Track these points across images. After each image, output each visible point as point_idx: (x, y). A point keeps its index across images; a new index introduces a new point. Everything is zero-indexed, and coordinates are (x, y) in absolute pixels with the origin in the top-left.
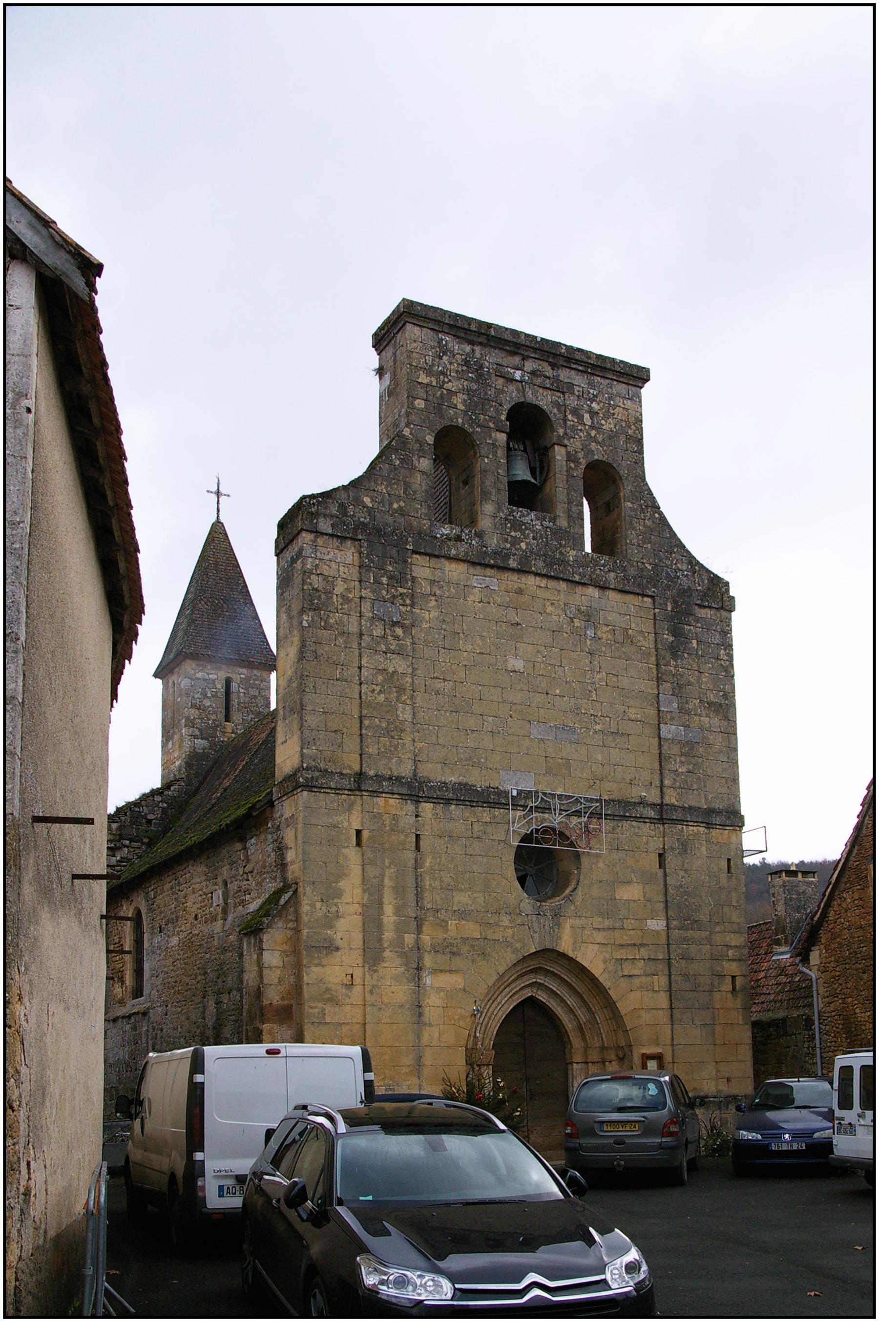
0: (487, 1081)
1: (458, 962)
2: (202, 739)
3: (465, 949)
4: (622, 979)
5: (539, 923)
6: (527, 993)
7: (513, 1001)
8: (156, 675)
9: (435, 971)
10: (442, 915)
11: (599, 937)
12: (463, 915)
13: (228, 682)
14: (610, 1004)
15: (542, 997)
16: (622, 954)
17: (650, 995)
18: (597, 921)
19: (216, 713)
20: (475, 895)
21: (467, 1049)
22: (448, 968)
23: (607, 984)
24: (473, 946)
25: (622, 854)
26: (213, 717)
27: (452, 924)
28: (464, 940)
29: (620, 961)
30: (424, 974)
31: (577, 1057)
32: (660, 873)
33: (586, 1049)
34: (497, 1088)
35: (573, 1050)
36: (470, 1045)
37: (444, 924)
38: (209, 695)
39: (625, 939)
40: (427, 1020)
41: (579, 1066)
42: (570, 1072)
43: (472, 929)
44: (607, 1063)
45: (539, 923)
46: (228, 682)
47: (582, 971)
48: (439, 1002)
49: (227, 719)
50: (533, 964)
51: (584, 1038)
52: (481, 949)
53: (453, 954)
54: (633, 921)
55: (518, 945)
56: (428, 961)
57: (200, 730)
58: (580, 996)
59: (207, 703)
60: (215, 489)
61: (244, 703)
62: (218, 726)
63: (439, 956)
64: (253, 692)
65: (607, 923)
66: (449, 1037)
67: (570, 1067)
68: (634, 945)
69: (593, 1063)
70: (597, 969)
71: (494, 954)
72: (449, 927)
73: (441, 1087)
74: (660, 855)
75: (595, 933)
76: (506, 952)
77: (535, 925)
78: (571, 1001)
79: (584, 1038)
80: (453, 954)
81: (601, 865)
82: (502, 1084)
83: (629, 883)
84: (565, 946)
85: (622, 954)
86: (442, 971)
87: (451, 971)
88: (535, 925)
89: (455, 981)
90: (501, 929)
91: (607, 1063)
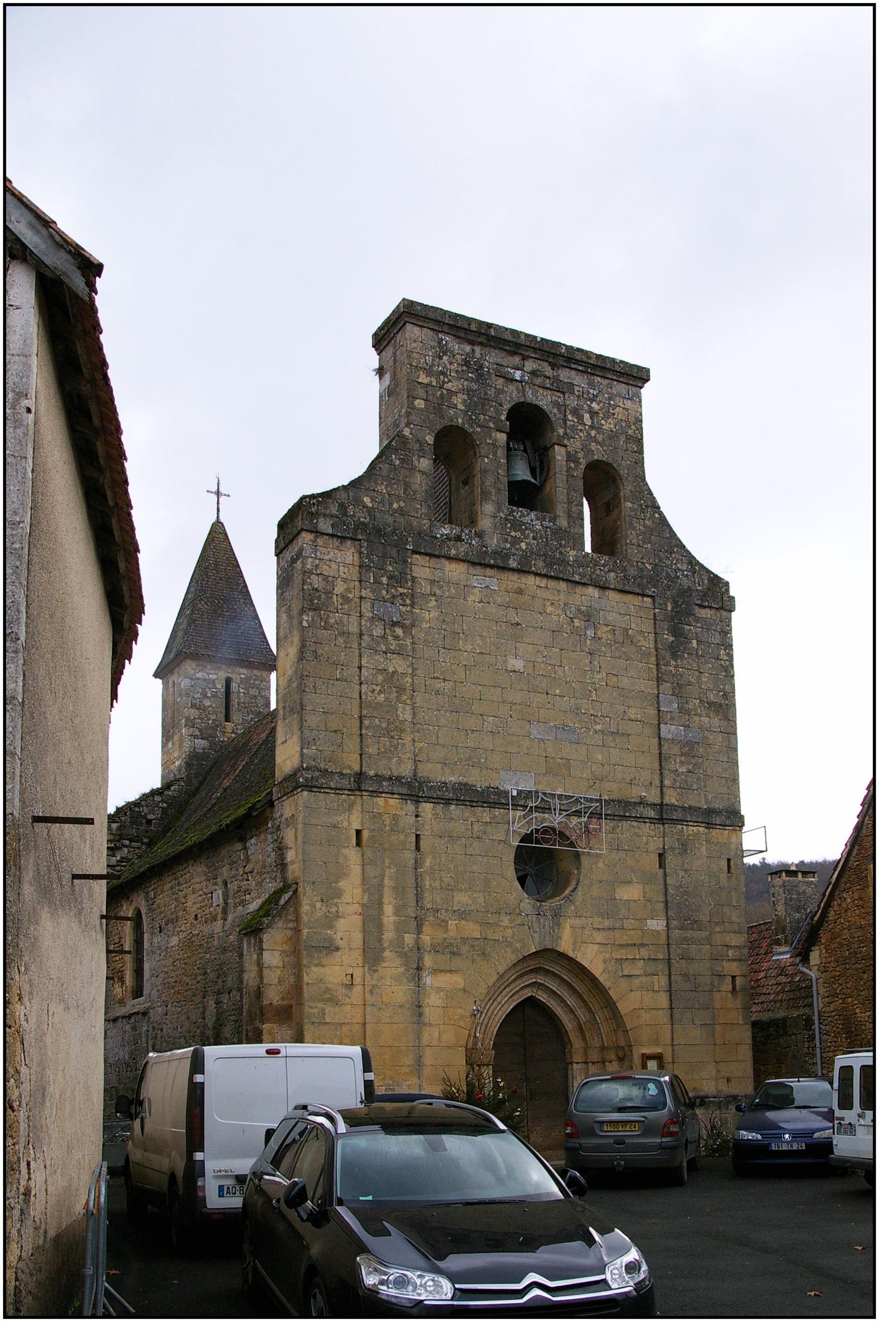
0: (487, 1081)
1: (458, 962)
2: (202, 739)
3: (465, 949)
4: (622, 979)
5: (539, 923)
6: (527, 993)
7: (513, 1001)
8: (156, 675)
9: (435, 971)
10: (442, 915)
11: (599, 937)
12: (463, 915)
13: (228, 682)
14: (610, 1005)
15: (542, 997)
16: (622, 954)
17: (650, 996)
18: (597, 921)
19: (216, 713)
20: (475, 895)
21: (467, 1049)
22: (448, 968)
23: (607, 984)
24: (473, 946)
25: (622, 854)
26: (213, 717)
27: (452, 924)
28: (464, 940)
29: (620, 961)
30: (424, 974)
31: (577, 1057)
32: (660, 872)
33: (586, 1049)
34: (497, 1088)
35: (573, 1051)
36: (470, 1045)
37: (444, 924)
38: (209, 695)
39: (626, 940)
40: (426, 1020)
41: (579, 1066)
42: (570, 1072)
43: (472, 929)
44: (607, 1063)
45: (539, 923)
46: (228, 682)
47: (582, 971)
48: (439, 1002)
49: (227, 719)
50: (533, 964)
51: (584, 1038)
52: (481, 949)
53: (453, 953)
54: (633, 921)
55: (518, 945)
56: (428, 961)
57: (200, 730)
58: (580, 997)
59: (207, 703)
60: (215, 489)
61: (244, 703)
62: (218, 726)
63: (439, 956)
64: (253, 692)
65: (607, 923)
66: (449, 1037)
67: (570, 1067)
68: (634, 945)
69: (593, 1063)
70: (597, 969)
71: (494, 955)
72: (449, 928)
73: (441, 1087)
74: (660, 855)
75: (595, 933)
76: (506, 952)
77: (535, 925)
78: (571, 1001)
79: (584, 1038)
80: (453, 953)
81: (601, 865)
82: (502, 1084)
83: (629, 883)
84: (565, 945)
85: (622, 954)
86: (441, 971)
87: (451, 971)
88: (535, 925)
89: (456, 981)
90: (501, 929)
91: (607, 1063)
